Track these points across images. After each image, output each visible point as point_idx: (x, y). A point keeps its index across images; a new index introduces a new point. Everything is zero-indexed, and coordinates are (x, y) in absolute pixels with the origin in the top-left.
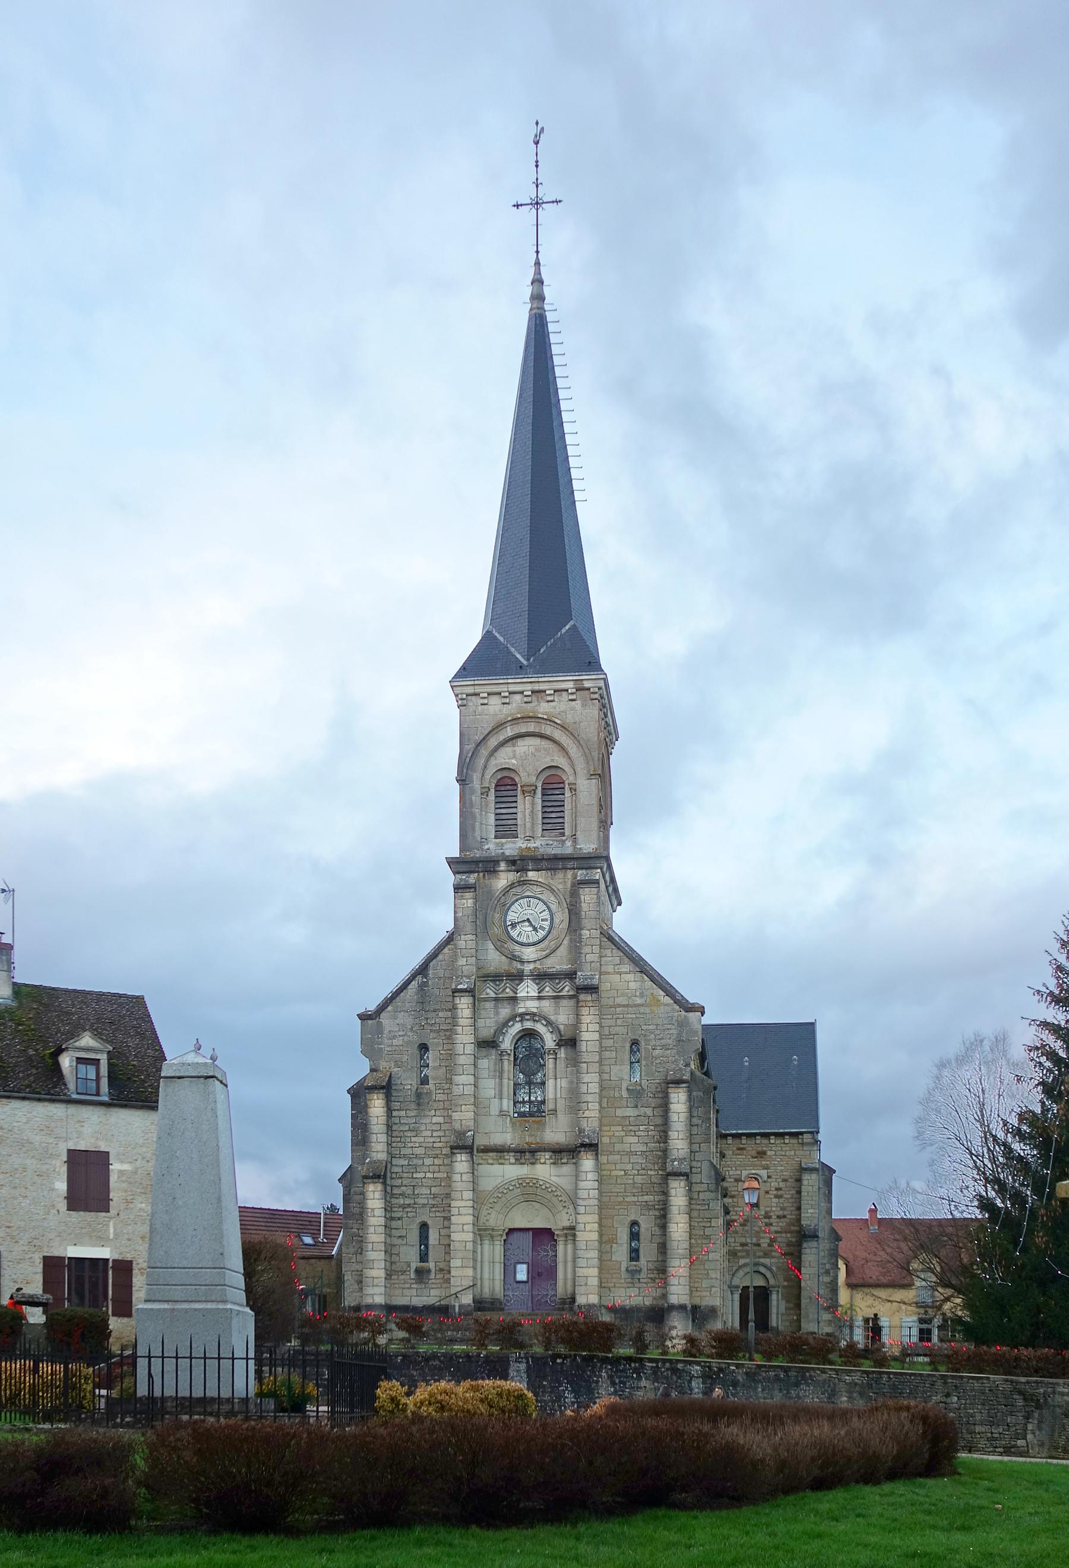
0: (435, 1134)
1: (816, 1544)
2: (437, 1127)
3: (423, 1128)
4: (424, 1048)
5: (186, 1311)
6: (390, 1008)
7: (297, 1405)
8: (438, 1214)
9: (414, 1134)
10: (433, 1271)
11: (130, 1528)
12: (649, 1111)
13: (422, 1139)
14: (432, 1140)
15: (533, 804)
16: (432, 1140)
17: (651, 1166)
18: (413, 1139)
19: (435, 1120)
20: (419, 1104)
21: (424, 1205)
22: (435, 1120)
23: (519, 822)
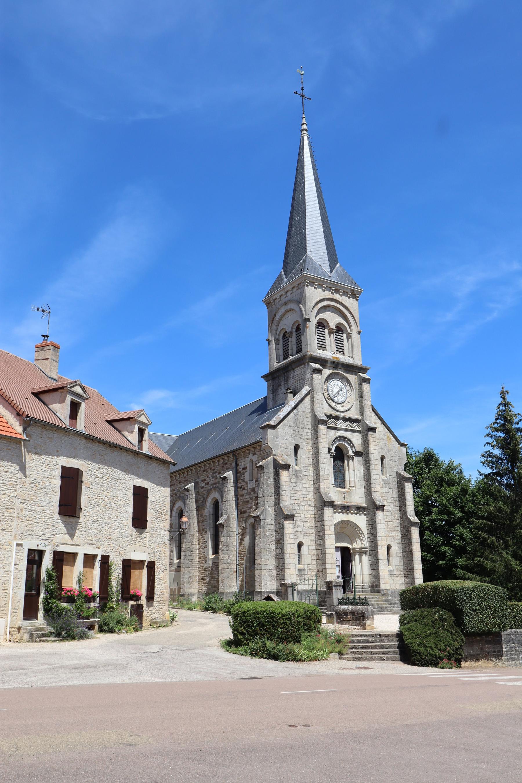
0: (304, 493)
1: (161, 607)
2: (305, 489)
3: (298, 489)
4: (297, 448)
5: (22, 450)
6: (282, 424)
7: (426, 632)
8: (307, 537)
9: (295, 492)
10: (306, 569)
11: (304, 608)
12: (391, 491)
13: (298, 496)
14: (303, 496)
15: (281, 568)
16: (303, 496)
17: (393, 517)
18: (295, 495)
19: (304, 485)
20: (296, 476)
21: (300, 532)
22: (304, 485)
23: (327, 344)
